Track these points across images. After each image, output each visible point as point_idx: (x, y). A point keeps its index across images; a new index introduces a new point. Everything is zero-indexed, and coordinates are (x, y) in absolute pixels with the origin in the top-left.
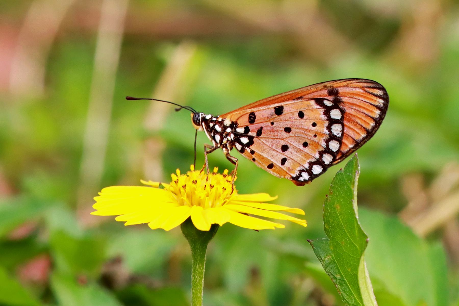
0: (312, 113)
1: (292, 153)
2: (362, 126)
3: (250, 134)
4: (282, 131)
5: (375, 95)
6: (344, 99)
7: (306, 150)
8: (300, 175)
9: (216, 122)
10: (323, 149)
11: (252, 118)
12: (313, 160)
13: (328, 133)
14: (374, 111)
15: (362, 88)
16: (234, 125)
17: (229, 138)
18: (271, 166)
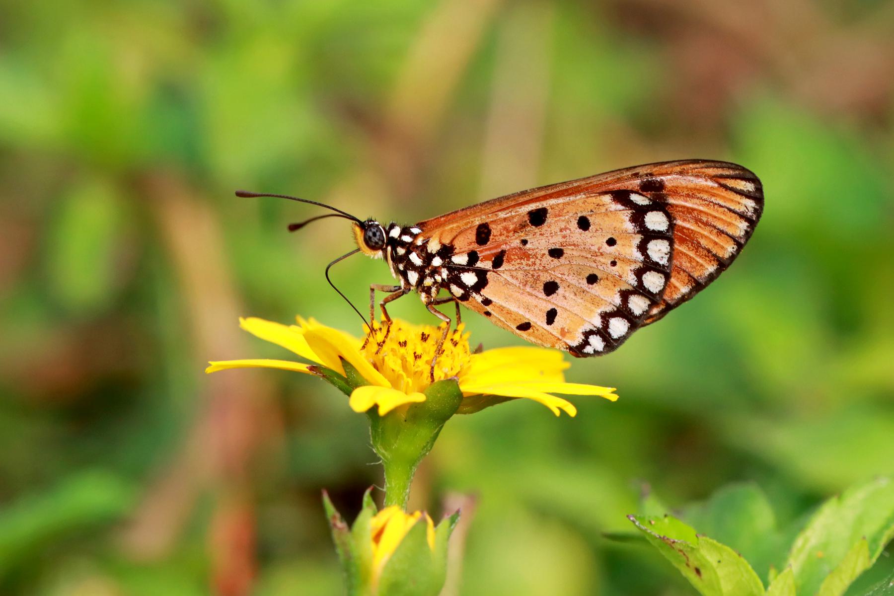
0: (606, 219)
1: (564, 297)
2: (709, 251)
3: (479, 264)
4: (544, 254)
7: (595, 289)
8: (586, 343)
9: (410, 248)
10: (630, 288)
11: (483, 234)
12: (609, 309)
13: (642, 258)
14: (733, 222)
15: (713, 178)
16: (446, 252)
17: (438, 278)
18: (525, 327)
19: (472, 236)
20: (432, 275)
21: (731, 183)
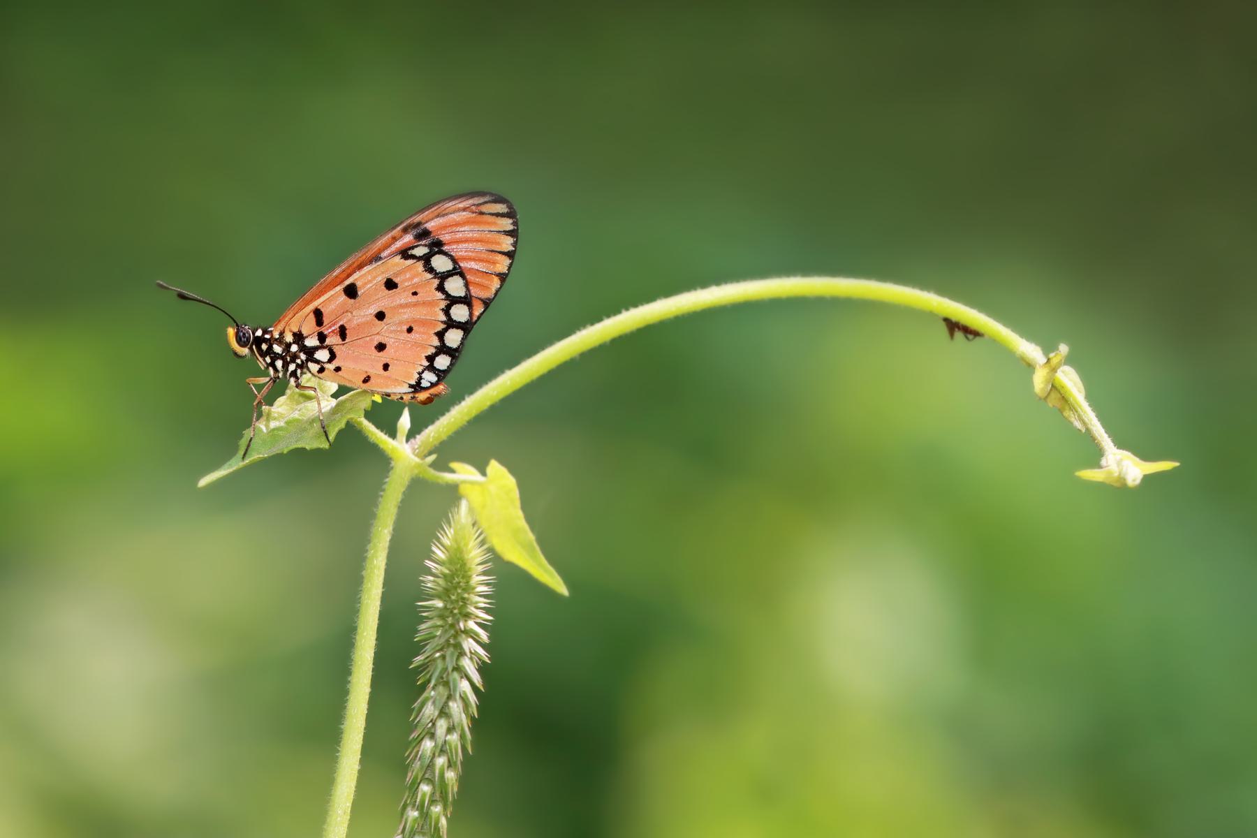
5: (498, 215)
6: (445, 238)
12: (432, 351)
17: (299, 361)
19: (312, 319)
20: (293, 361)
21: (485, 209)
